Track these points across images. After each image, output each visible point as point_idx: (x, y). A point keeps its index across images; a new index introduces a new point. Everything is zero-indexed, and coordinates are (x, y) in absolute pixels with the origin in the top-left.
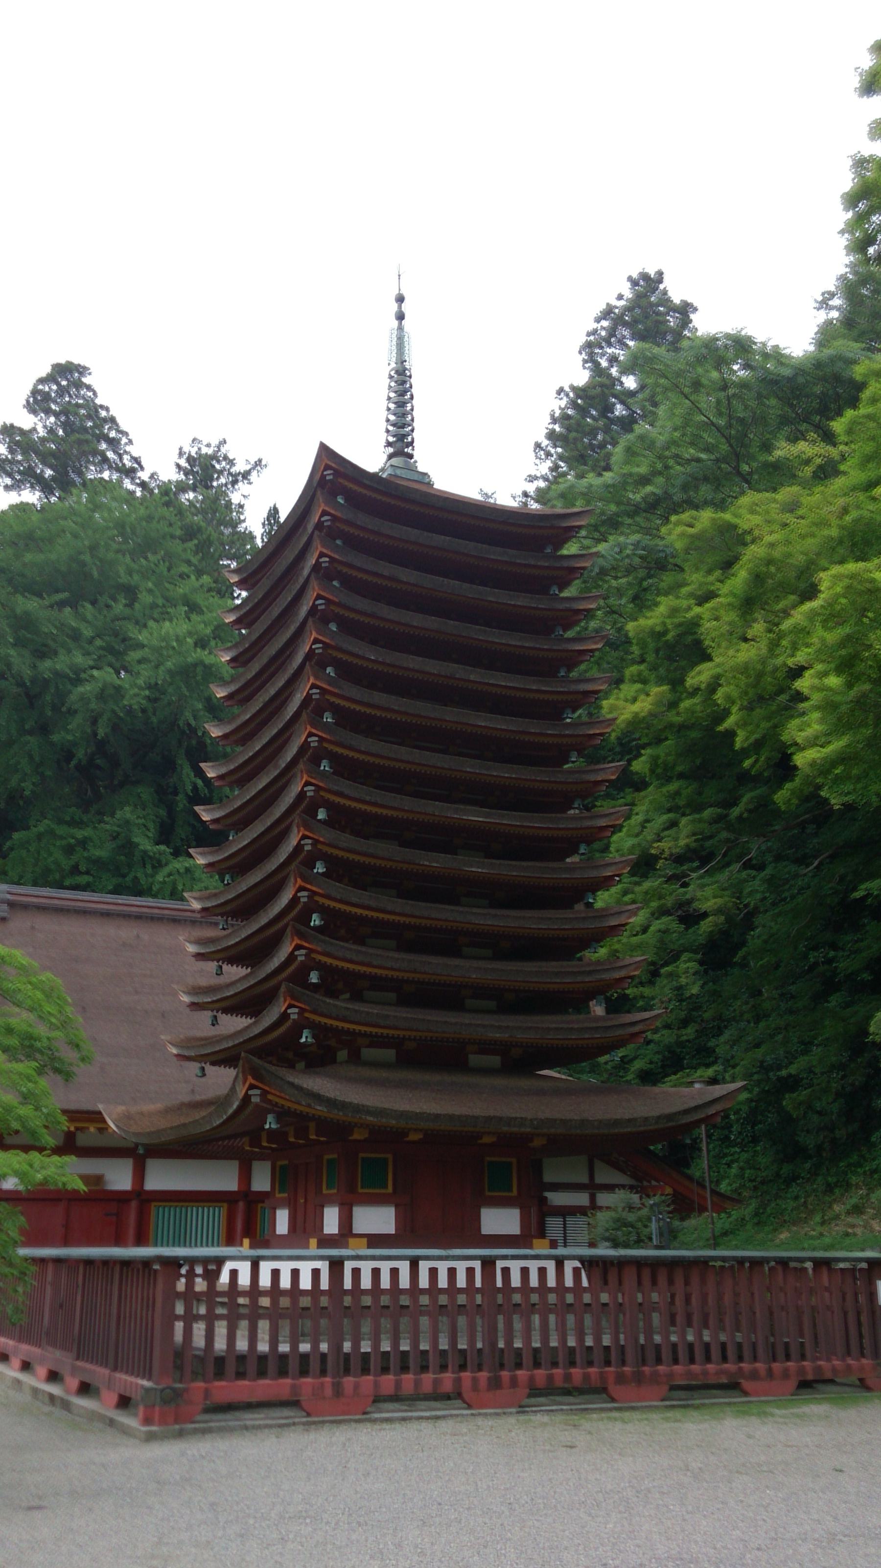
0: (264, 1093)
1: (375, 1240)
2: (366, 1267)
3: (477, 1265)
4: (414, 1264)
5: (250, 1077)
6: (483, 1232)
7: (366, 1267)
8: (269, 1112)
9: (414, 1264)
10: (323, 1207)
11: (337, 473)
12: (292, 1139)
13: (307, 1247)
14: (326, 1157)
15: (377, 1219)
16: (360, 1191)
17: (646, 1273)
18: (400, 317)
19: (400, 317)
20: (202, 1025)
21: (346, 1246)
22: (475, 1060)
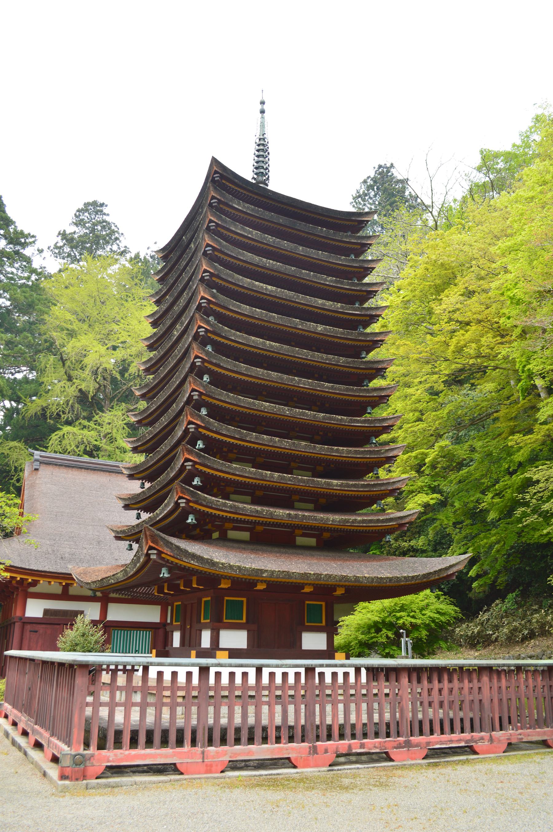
0: (160, 553)
1: (234, 653)
2: (225, 673)
3: (302, 671)
4: (259, 670)
5: (149, 542)
6: (325, 648)
7: (225, 673)
8: (163, 566)
9: (259, 670)
10: (201, 631)
11: (222, 176)
12: (182, 588)
13: (189, 657)
14: (204, 599)
15: (236, 639)
16: (225, 621)
17: (414, 676)
18: (262, 112)
19: (262, 112)
20: (130, 518)
21: (214, 657)
22: (300, 541)
